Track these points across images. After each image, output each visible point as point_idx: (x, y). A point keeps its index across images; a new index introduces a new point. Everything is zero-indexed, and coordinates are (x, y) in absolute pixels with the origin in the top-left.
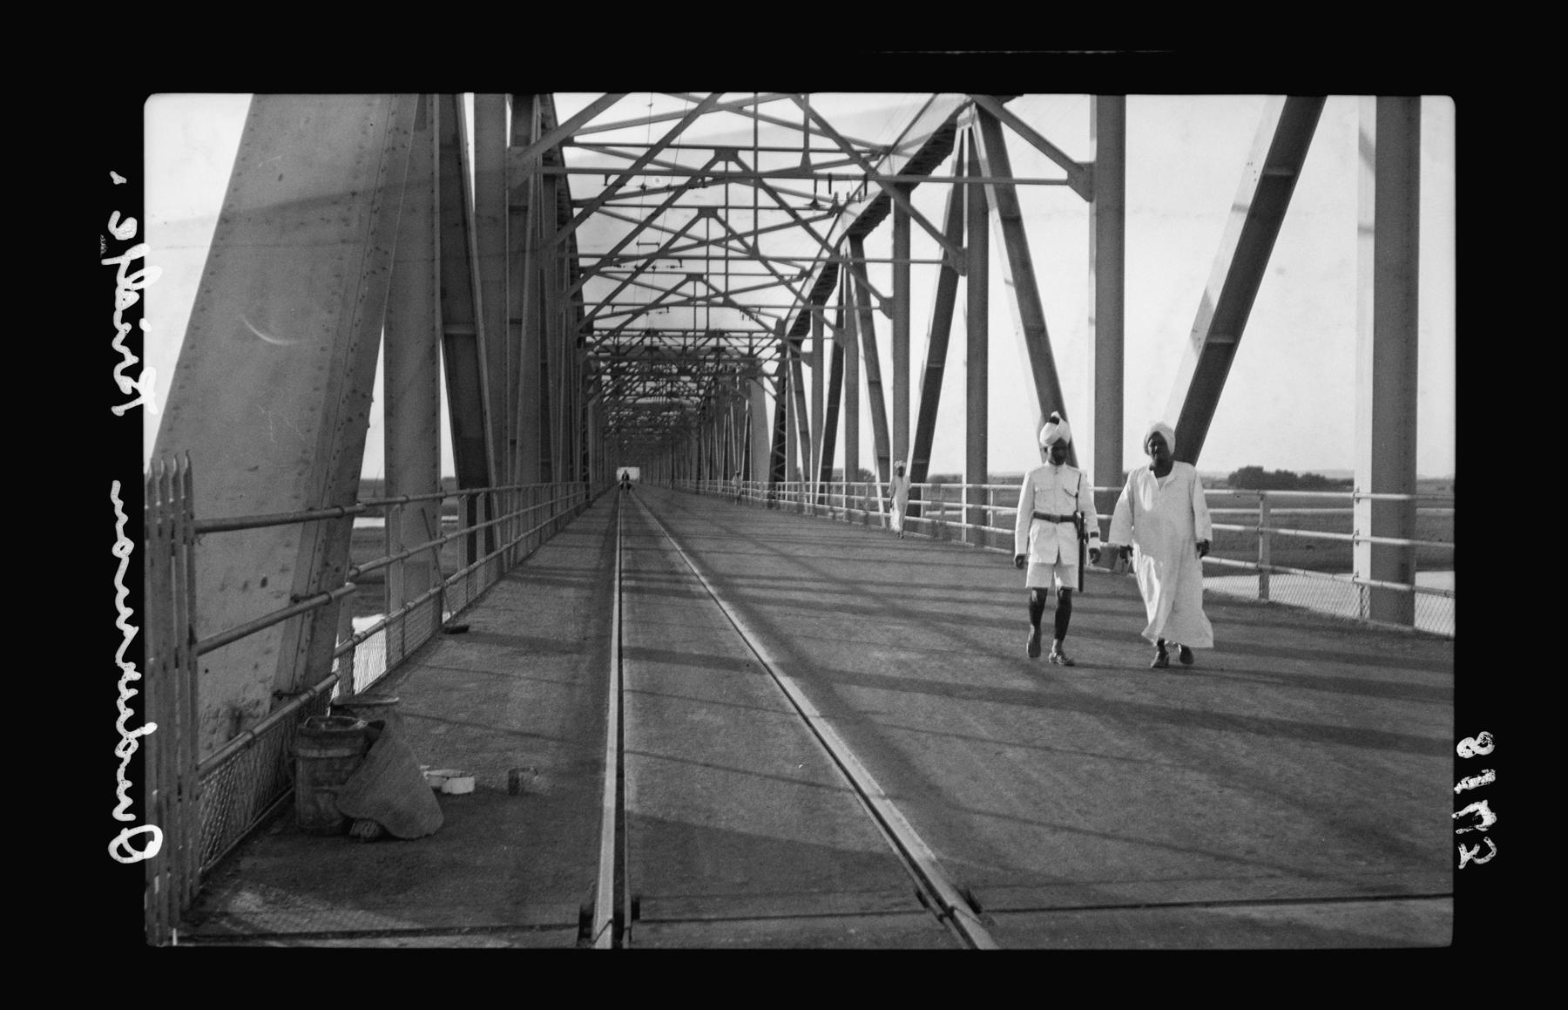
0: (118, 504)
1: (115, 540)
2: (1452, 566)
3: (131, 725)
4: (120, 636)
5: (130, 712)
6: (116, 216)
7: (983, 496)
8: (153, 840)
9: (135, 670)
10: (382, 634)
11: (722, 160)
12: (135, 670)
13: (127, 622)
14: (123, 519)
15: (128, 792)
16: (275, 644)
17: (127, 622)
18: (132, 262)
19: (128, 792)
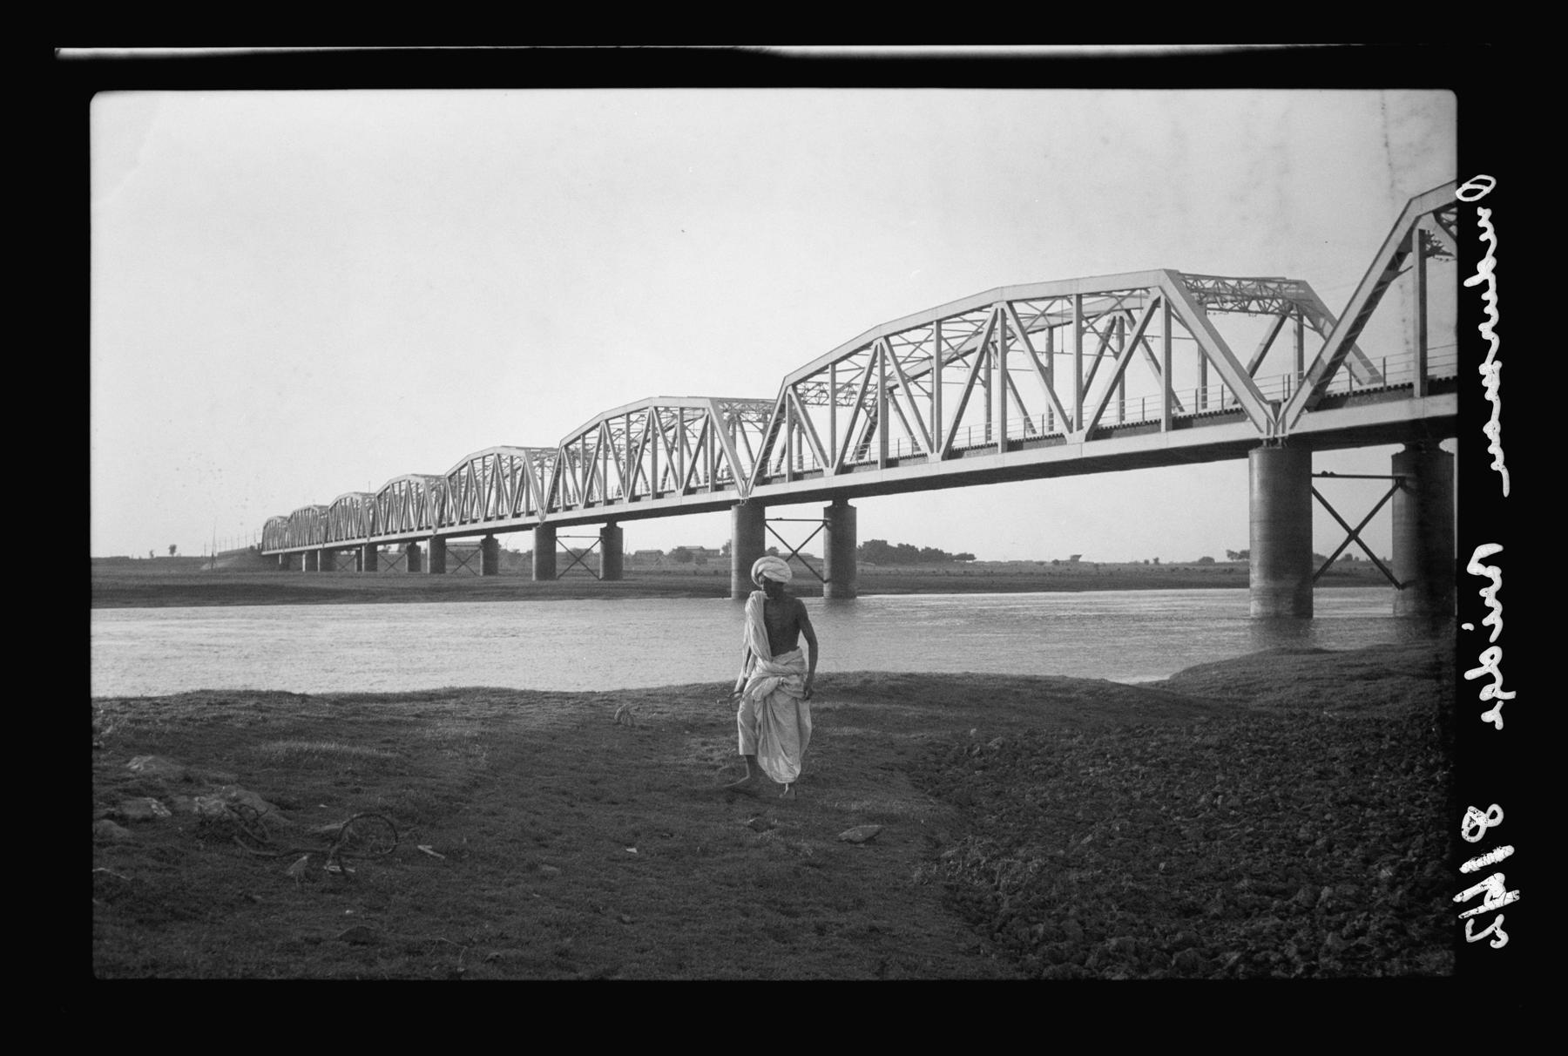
0: (1495, 449)
1: (1500, 666)
2: (93, 561)
3: (1484, 286)
4: (1499, 596)
5: (1485, 297)
6: (1495, 548)
7: (463, 925)
8: (1411, 251)
9: (1485, 598)
10: (1337, 318)
11: (1310, 482)
12: (1485, 598)
13: (1491, 609)
14: (1492, 429)
15: (1493, 458)
16: (1411, 276)
17: (1491, 609)
18: (1487, 566)
19: (1493, 458)
